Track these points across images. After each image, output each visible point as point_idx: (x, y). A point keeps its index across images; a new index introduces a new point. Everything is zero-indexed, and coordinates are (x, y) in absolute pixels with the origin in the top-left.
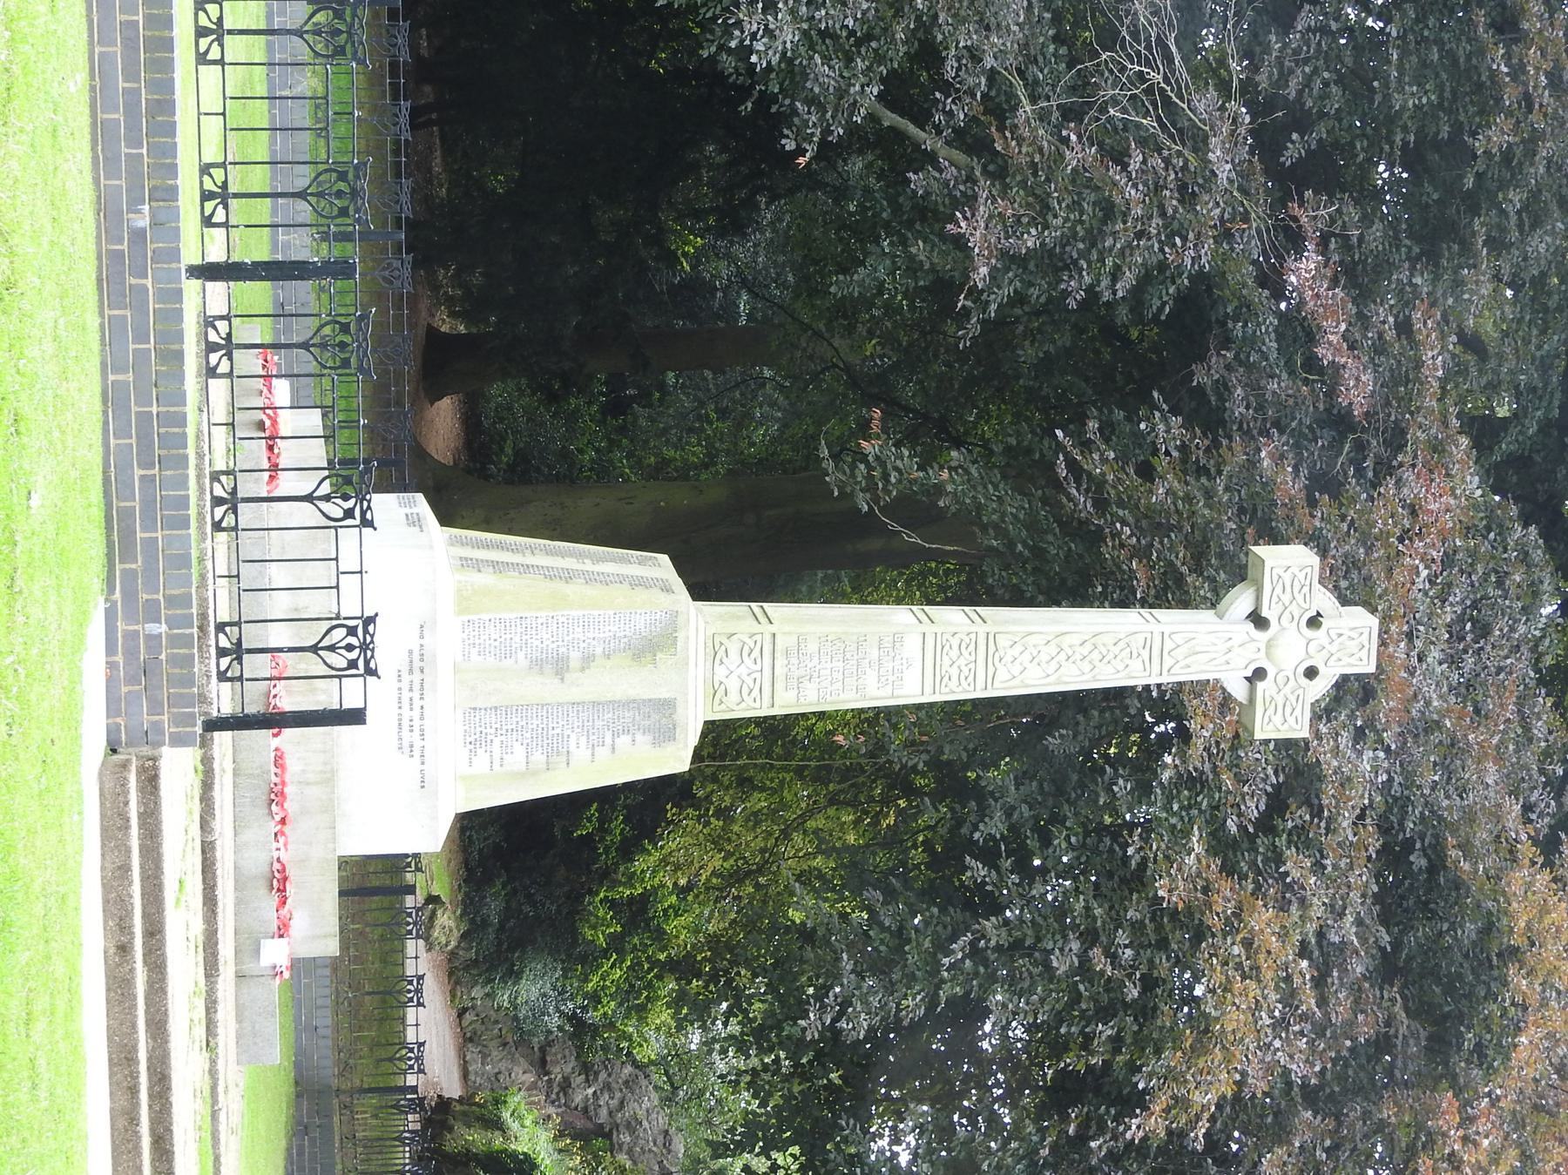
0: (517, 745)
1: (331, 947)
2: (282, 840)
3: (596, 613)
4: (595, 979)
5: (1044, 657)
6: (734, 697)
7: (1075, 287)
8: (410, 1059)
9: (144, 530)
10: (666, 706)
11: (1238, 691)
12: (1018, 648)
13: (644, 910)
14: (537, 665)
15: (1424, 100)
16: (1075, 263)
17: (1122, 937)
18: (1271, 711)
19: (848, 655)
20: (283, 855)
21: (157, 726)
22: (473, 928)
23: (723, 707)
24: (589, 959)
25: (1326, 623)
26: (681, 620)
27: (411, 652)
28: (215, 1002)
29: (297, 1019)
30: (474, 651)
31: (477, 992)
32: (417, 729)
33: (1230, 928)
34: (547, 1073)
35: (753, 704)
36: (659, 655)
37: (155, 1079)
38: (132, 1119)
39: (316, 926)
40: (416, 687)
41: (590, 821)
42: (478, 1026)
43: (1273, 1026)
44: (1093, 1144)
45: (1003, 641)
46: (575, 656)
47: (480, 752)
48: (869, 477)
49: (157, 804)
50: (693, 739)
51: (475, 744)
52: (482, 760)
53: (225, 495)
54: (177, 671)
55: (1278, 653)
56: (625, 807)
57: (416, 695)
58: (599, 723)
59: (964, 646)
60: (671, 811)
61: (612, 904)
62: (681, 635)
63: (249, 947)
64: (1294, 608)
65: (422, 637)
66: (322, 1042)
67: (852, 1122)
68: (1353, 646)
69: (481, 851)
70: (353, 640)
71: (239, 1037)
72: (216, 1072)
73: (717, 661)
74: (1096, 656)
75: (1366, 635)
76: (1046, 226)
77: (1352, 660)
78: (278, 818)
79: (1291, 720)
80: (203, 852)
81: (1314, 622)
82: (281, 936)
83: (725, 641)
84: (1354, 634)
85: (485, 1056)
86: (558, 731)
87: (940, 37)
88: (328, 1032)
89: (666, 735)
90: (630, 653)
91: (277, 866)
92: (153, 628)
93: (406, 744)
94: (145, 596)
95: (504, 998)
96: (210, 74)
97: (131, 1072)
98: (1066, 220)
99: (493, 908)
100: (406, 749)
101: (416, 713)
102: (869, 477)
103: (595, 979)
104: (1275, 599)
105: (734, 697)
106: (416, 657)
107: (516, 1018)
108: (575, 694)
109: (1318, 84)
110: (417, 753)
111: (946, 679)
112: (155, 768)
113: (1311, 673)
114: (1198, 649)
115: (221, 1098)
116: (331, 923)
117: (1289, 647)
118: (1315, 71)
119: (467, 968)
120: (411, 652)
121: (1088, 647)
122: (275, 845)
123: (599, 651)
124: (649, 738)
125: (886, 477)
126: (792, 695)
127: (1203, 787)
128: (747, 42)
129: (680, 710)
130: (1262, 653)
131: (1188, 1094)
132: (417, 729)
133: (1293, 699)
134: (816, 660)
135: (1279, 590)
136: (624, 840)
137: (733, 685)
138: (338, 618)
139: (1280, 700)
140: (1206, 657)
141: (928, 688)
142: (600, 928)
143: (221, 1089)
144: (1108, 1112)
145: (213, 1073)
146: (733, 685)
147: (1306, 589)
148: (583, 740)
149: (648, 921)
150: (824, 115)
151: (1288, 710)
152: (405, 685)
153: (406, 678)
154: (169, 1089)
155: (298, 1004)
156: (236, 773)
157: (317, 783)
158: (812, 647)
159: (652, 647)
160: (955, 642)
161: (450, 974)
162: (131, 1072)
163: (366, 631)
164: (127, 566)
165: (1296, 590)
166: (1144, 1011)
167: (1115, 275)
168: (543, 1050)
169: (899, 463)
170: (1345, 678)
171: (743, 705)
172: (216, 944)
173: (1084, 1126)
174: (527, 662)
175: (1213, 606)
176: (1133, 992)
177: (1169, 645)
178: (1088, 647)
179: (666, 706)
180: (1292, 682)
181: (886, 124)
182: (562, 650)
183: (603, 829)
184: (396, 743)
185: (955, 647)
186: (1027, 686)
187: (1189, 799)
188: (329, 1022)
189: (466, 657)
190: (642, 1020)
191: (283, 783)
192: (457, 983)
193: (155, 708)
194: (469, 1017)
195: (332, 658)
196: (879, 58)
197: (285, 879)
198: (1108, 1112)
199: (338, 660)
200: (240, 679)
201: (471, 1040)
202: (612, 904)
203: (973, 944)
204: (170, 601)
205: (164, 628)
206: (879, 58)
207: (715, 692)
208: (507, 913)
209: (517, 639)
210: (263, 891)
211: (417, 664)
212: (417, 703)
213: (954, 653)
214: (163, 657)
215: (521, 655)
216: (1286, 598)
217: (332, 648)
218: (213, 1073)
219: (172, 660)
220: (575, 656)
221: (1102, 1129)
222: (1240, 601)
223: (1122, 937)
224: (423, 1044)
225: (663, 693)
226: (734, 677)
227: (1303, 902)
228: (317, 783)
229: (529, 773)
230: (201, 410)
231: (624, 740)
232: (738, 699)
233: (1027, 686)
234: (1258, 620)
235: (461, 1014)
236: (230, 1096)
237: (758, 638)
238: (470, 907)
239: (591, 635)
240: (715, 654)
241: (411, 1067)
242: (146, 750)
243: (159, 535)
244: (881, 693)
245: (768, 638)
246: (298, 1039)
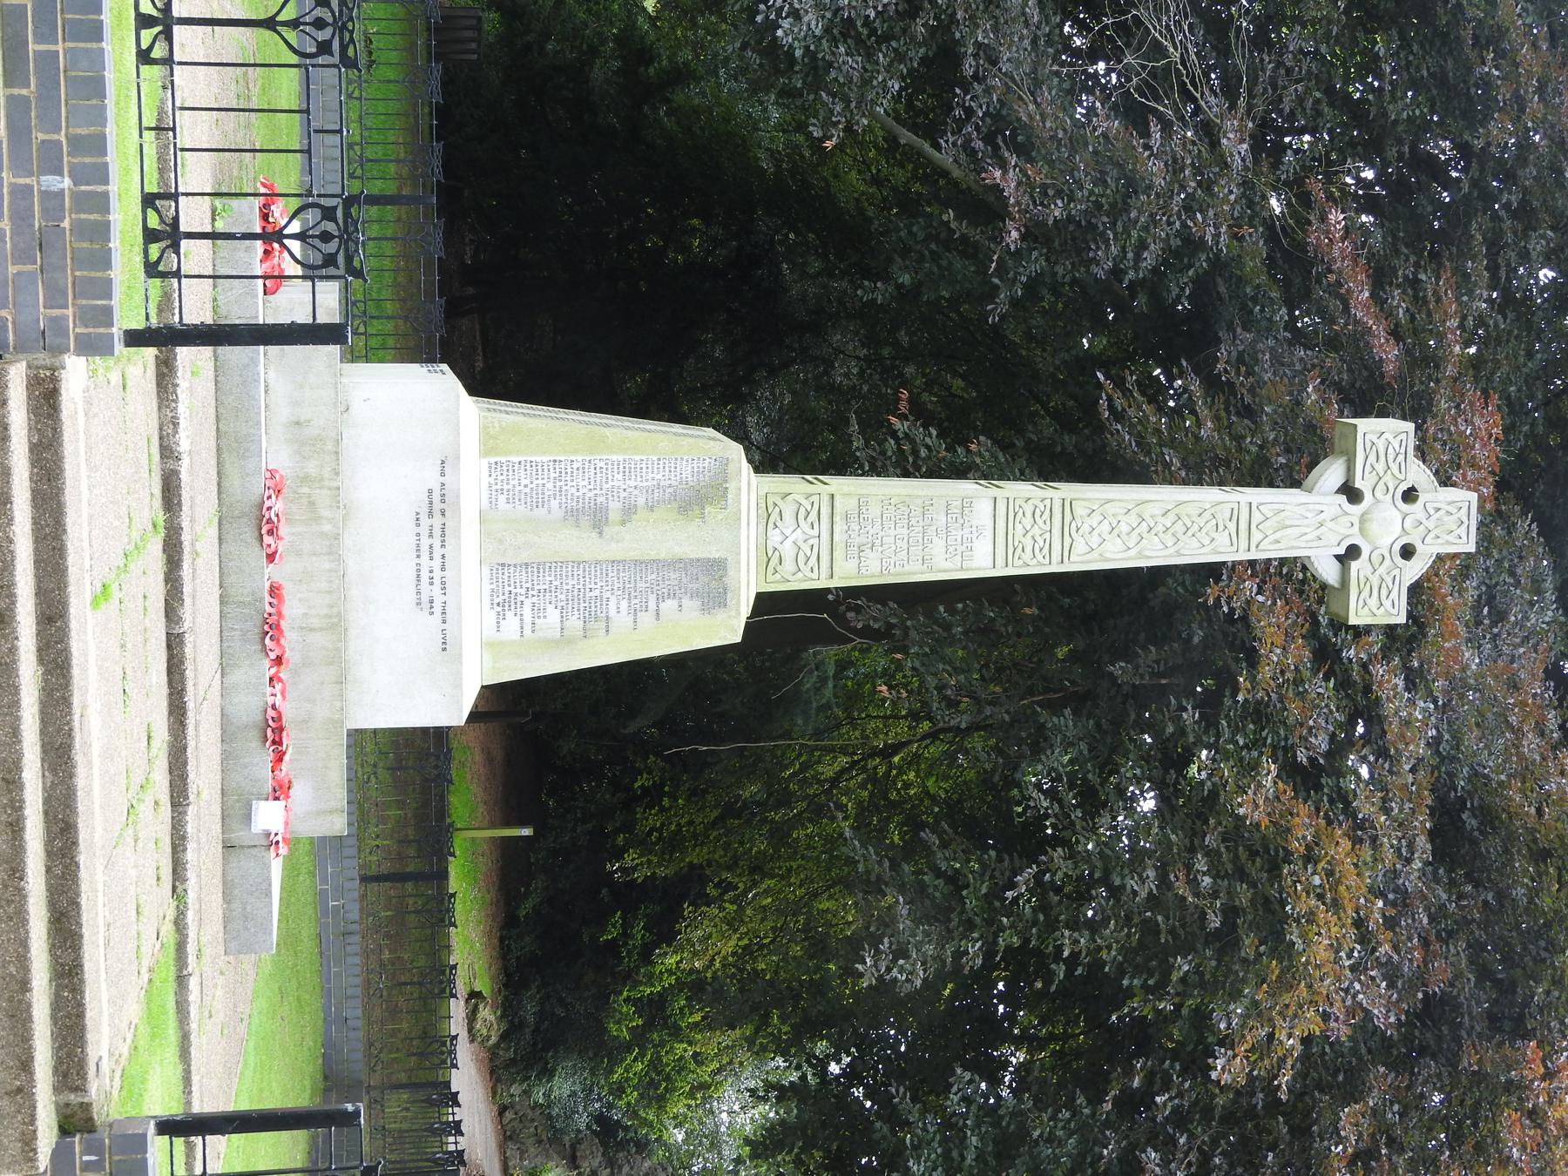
0: (550, 608)
1: (338, 825)
2: (278, 686)
3: (638, 458)
4: (620, 1071)
5: (1124, 528)
6: (789, 566)
7: (1104, 258)
9: (35, 42)
10: (716, 568)
11: (1328, 571)
12: (1097, 517)
13: (663, 1009)
14: (573, 515)
15: (1417, 112)
16: (1103, 234)
17: (1201, 864)
19: (913, 522)
20: (278, 700)
21: (58, 325)
22: (512, 1028)
23: (778, 576)
24: (611, 1053)
25: (1423, 497)
26: (731, 468)
27: (430, 491)
28: (184, 838)
29: (326, 1009)
30: (502, 499)
31: (516, 1089)
32: (437, 581)
33: (1309, 858)
34: (577, 1167)
35: (809, 574)
36: (708, 509)
37: (56, 829)
38: (14, 870)
39: (318, 800)
40: (437, 532)
41: (614, 926)
42: (516, 1124)
43: (1353, 968)
44: (1158, 1099)
45: (1080, 510)
46: (615, 506)
47: (509, 615)
48: (900, 450)
49: (56, 430)
50: (746, 610)
51: (505, 604)
52: (511, 624)
53: (155, 13)
54: (85, 245)
55: (1373, 527)
56: (645, 916)
57: (437, 543)
58: (641, 585)
59: (1038, 513)
60: (687, 909)
61: (636, 1002)
62: (731, 486)
63: (236, 811)
64: (1388, 478)
65: (443, 474)
66: (352, 1035)
67: (902, 1090)
68: (1451, 523)
69: (518, 958)
70: (330, 227)
71: (227, 921)
72: (185, 927)
73: (771, 525)
74: (1179, 527)
75: (1464, 510)
76: (1071, 199)
77: (1450, 538)
78: (273, 656)
79: (1387, 604)
80: (169, 647)
81: (1410, 495)
82: (277, 799)
83: (779, 502)
84: (1452, 509)
85: (522, 1153)
86: (597, 593)
87: (958, 35)
88: (359, 1023)
89: (716, 599)
90: (675, 505)
91: (270, 711)
92: (51, 182)
93: (425, 599)
94: (41, 136)
95: (539, 1096)
97: (12, 801)
98: (1091, 193)
99: (529, 1010)
102: (900, 450)
103: (620, 1071)
104: (1368, 468)
105: (789, 566)
106: (436, 497)
107: (550, 1117)
108: (615, 550)
109: (1309, 104)
110: (437, 609)
111: (1019, 550)
112: (55, 380)
113: (1407, 552)
114: (1288, 522)
115: (191, 959)
116: (338, 794)
117: (1386, 524)
118: (1308, 90)
119: (506, 1068)
120: (430, 491)
121: (1171, 517)
122: (269, 690)
123: (641, 501)
124: (696, 603)
125: (915, 453)
126: (853, 564)
127: (1268, 721)
128: (773, 17)
129: (731, 573)
131: (1259, 1040)
132: (437, 581)
133: (1389, 580)
134: (878, 526)
135: (1372, 458)
136: (645, 945)
137: (788, 550)
138: (310, 194)
139: (1375, 582)
140: (1297, 531)
141: (1000, 561)
142: (623, 1023)
143: (191, 948)
144: (1172, 1067)
145: (180, 924)
146: (788, 550)
147: (1401, 457)
148: (624, 604)
149: (666, 1019)
150: (848, 106)
151: (1384, 592)
152: (424, 530)
154: (75, 843)
155: (327, 994)
156: (223, 600)
157: (321, 629)
158: (874, 511)
159: (701, 498)
160: (1029, 509)
161: (492, 1072)
162: (12, 801)
163: (347, 215)
164: (16, 91)
165: (1391, 457)
166: (1226, 940)
167: (1142, 245)
168: (573, 1148)
169: (928, 440)
170: (1440, 558)
171: (800, 575)
172: (185, 763)
173: (1150, 1077)
174: (561, 513)
175: (1296, 484)
176: (1215, 922)
177: (1257, 517)
178: (1171, 517)
179: (716, 568)
180: (1388, 562)
181: (902, 142)
182: (599, 500)
183: (626, 935)
185: (1029, 515)
186: (1107, 560)
187: (1255, 732)
188: (359, 1013)
189: (493, 503)
190: (661, 1108)
191: (280, 614)
192: (498, 1080)
193: (56, 297)
194: (509, 1115)
196: (900, 57)
197: (281, 729)
198: (1172, 1067)
200: (177, 274)
201: (510, 1138)
202: (636, 1002)
203: (1038, 878)
204: (74, 141)
205: (67, 183)
206: (900, 57)
207: (768, 559)
208: (541, 1015)
209: (550, 485)
210: (255, 744)
211: (437, 506)
212: (438, 551)
213: (1028, 521)
214: (66, 224)
215: (554, 504)
216: (1380, 467)
218: (180, 924)
219: (80, 229)
220: (615, 506)
221: (1166, 1087)
222: (1330, 474)
223: (1201, 864)
226: (788, 542)
227: (1374, 839)
228: (321, 629)
229: (564, 640)
230: (164, 87)
231: (669, 605)
232: (793, 568)
233: (1107, 560)
234: (1350, 492)
235: (502, 1111)
236: (205, 960)
237: (813, 498)
238: (509, 1009)
239: (633, 483)
240: (768, 515)
242: (42, 358)
243: (60, 47)
244: (949, 565)
245: (826, 499)
246: (327, 1032)
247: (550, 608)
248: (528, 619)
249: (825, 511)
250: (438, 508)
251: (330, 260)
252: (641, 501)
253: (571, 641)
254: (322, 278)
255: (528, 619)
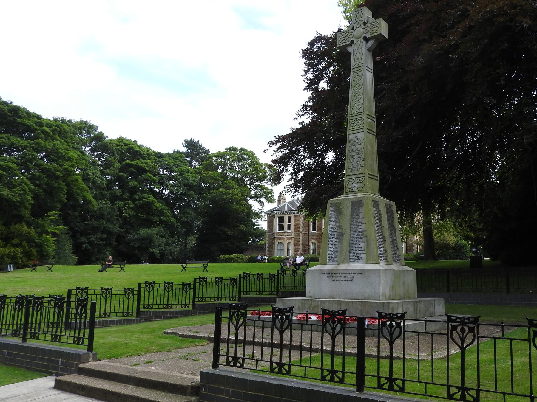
0: (360, 246)
8: (282, 318)
11: (371, 43)
18: (374, 31)
32: (346, 276)
40: (336, 275)
57: (339, 275)
58: (356, 223)
62: (336, 202)
70: (459, 328)
93: (350, 279)
96: (154, 307)
100: (351, 279)
101: (342, 275)
106: (329, 275)
108: (348, 230)
110: (352, 275)
123: (338, 224)
129: (355, 200)
130: (359, 40)
132: (346, 276)
135: (344, 41)
141: (376, 178)
148: (360, 227)
153: (334, 278)
163: (454, 321)
184: (349, 282)
195: (131, 296)
199: (108, 295)
211: (330, 275)
212: (340, 275)
215: (337, 246)
216: (346, 38)
217: (129, 296)
224: (380, 314)
225: (350, 205)
226: (356, 185)
231: (361, 215)
241: (287, 317)
247: (360, 246)
248: (362, 252)
249: (350, 177)
250: (331, 274)
251: (471, 330)
252: (338, 224)
253: (367, 240)
254: (478, 333)
255: (362, 252)
